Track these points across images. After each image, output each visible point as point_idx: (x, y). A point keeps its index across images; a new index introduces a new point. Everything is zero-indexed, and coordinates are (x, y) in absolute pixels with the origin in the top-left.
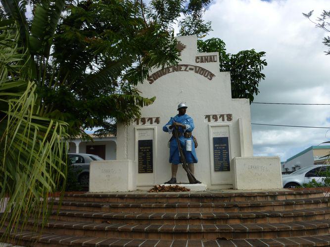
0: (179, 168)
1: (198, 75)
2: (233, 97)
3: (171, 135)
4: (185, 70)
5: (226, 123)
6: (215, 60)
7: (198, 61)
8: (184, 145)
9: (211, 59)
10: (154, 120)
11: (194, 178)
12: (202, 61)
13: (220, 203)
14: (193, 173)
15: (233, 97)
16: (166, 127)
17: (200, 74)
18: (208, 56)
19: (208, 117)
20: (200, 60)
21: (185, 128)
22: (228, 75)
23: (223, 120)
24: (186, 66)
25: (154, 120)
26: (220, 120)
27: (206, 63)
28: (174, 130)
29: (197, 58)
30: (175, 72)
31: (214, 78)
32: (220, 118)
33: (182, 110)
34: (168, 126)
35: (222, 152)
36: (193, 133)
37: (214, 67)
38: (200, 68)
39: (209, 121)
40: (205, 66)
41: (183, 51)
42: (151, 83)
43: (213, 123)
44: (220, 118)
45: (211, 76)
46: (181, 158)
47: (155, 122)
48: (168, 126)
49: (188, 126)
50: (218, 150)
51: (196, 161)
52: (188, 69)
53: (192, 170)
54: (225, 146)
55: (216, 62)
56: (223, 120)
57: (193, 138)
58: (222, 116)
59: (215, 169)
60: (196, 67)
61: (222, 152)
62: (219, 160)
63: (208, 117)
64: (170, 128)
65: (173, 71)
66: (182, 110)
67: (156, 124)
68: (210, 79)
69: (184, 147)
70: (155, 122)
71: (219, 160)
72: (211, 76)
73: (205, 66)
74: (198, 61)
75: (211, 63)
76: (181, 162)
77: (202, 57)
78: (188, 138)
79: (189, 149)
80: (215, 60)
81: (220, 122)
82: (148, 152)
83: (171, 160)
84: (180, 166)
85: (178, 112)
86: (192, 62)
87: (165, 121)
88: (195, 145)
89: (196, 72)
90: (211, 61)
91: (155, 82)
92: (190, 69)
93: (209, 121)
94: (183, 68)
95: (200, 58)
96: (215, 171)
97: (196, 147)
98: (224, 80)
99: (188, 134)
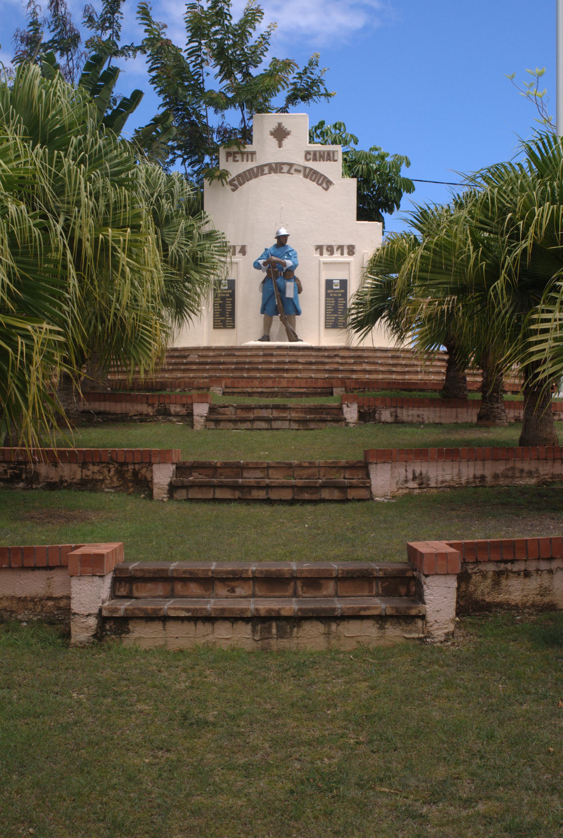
0: (273, 322)
1: (308, 180)
2: (358, 219)
3: (265, 274)
4: (289, 172)
5: (346, 258)
6: (335, 159)
7: (308, 158)
8: (282, 288)
9: (329, 157)
10: (238, 249)
11: (294, 333)
12: (315, 159)
13: (321, 353)
14: (294, 326)
15: (358, 219)
16: (259, 264)
17: (311, 179)
18: (324, 152)
19: (319, 248)
20: (311, 156)
21: (285, 265)
22: (353, 183)
23: (342, 254)
24: (291, 165)
25: (238, 249)
26: (337, 254)
27: (322, 162)
28: (269, 268)
29: (308, 153)
30: (273, 174)
31: (331, 188)
32: (337, 250)
33: (282, 240)
34: (261, 262)
35: (337, 301)
36: (297, 273)
37: (333, 169)
38: (311, 169)
39: (321, 254)
40: (320, 167)
41: (286, 139)
42: (233, 190)
43: (326, 257)
44: (337, 250)
45: (325, 183)
46: (280, 304)
47: (240, 252)
48: (261, 262)
49: (289, 263)
50: (331, 297)
51: (298, 313)
52: (292, 171)
53: (293, 325)
54: (230, 293)
55: (336, 161)
56: (342, 254)
57: (296, 279)
58: (341, 248)
59: (326, 325)
60: (305, 168)
61: (337, 301)
62: (333, 313)
63: (319, 248)
64: (265, 264)
65: (270, 173)
66: (282, 240)
67: (241, 255)
68: (326, 189)
69: (282, 291)
70: (240, 252)
71: (333, 313)
72: (325, 183)
73: (320, 167)
74: (308, 158)
75: (329, 162)
76: (277, 314)
77: (315, 153)
78: (289, 280)
79: (290, 294)
80: (335, 159)
81: (337, 257)
82: (228, 297)
83: (263, 311)
84: (276, 319)
85: (275, 241)
86: (300, 160)
87: (256, 252)
88: (299, 289)
89: (305, 176)
90: (329, 159)
91: (240, 188)
92: (296, 170)
93: (321, 254)
94: (286, 168)
95: (312, 153)
96: (326, 328)
97: (299, 292)
98: (347, 190)
99: (289, 274)
